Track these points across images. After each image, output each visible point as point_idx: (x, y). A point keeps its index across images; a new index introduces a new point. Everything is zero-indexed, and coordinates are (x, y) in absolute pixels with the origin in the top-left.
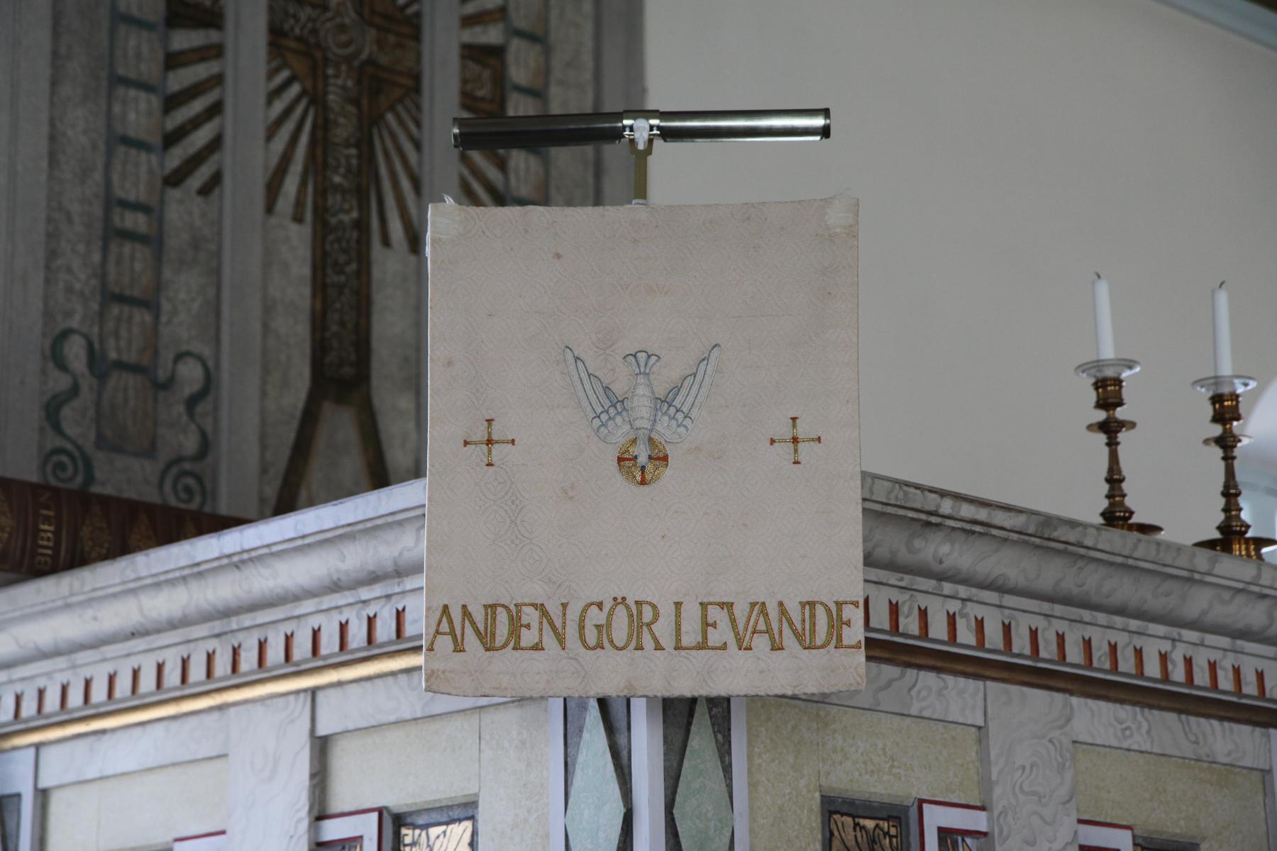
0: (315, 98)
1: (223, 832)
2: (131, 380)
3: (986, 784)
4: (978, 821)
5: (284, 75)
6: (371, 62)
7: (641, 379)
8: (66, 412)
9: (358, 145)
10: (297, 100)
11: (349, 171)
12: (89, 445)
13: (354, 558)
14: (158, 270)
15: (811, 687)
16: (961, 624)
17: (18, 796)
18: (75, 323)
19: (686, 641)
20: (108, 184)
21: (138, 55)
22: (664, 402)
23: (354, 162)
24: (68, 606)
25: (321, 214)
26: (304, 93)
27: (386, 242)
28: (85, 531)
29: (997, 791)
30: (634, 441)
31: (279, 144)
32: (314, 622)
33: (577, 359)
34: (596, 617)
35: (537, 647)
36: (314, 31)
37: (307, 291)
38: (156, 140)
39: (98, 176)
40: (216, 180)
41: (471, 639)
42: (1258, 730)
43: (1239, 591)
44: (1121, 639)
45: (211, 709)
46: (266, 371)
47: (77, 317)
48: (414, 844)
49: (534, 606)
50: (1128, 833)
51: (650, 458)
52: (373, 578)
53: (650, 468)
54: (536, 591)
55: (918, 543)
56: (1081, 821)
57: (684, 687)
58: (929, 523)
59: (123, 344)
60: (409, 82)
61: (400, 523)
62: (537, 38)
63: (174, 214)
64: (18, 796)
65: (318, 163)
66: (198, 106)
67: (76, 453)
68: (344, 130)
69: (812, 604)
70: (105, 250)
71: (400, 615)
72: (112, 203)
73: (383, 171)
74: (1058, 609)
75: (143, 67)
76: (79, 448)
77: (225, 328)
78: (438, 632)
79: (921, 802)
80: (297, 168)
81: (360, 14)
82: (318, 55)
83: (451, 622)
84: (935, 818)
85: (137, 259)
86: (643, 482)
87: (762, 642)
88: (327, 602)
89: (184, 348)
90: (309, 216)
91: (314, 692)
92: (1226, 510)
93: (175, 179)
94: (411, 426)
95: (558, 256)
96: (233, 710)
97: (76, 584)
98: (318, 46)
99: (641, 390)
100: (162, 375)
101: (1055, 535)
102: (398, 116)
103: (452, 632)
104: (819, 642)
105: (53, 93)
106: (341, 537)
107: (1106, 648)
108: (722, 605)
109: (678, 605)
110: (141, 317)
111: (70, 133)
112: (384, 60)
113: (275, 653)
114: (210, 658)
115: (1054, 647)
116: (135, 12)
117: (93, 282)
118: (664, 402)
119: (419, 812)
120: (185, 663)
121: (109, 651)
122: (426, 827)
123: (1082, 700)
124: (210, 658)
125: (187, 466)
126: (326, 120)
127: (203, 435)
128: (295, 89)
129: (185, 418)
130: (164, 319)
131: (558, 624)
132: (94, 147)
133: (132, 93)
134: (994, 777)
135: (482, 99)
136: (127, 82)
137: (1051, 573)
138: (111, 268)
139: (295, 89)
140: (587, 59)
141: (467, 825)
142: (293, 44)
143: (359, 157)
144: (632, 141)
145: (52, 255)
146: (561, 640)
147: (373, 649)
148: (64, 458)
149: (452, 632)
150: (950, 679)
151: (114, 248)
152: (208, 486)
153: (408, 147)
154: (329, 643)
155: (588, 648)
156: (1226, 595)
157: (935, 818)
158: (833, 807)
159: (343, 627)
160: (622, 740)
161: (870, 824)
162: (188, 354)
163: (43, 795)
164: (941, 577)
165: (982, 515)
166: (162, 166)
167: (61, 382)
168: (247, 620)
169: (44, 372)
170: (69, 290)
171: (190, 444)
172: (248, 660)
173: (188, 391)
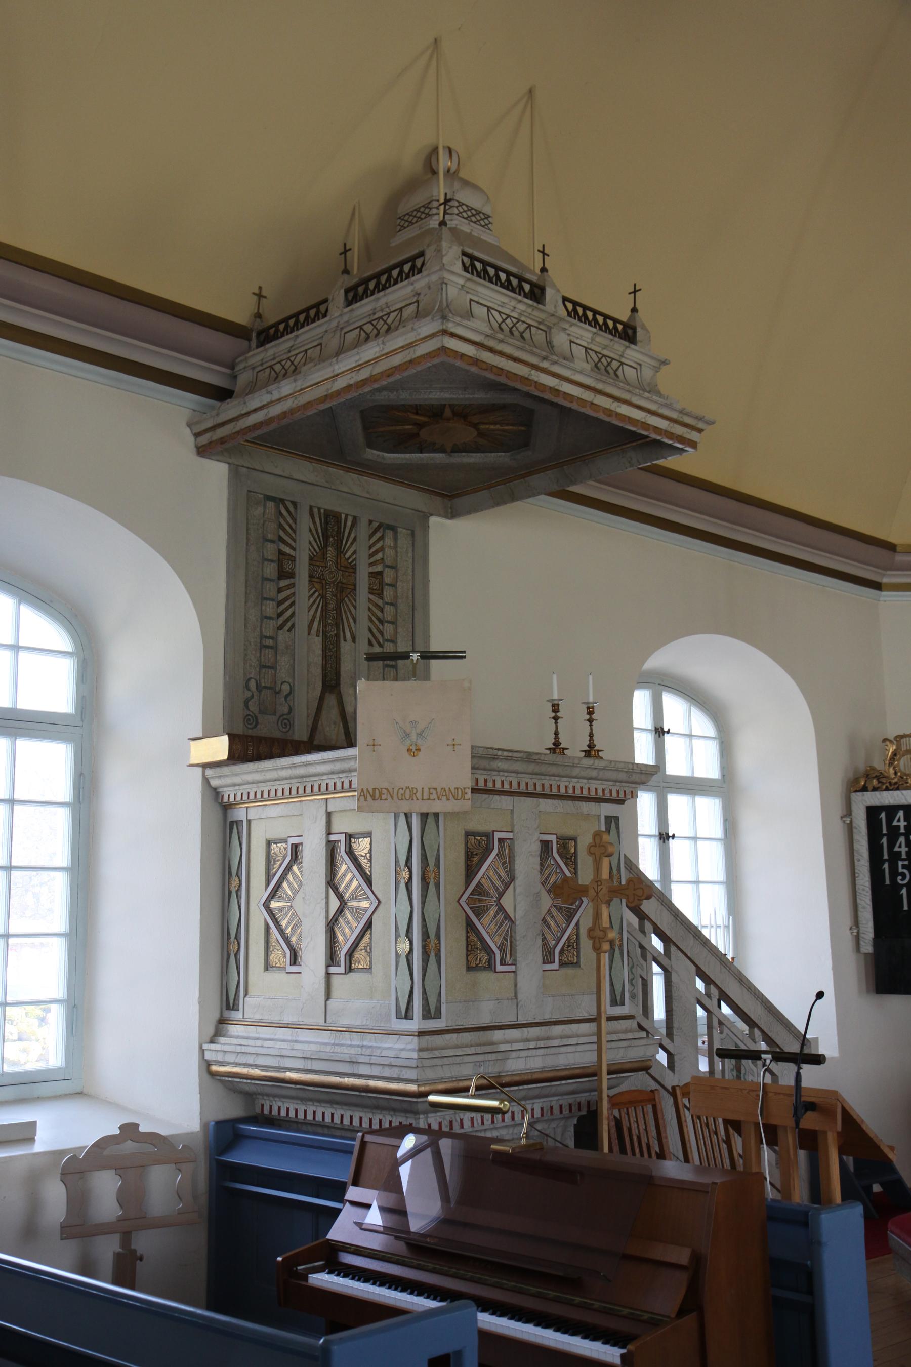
0: (323, 597)
1: (302, 836)
2: (268, 692)
3: (513, 825)
4: (510, 836)
5: (314, 590)
6: (340, 582)
7: (414, 728)
8: (250, 703)
9: (336, 610)
10: (318, 597)
11: (333, 618)
12: (257, 712)
13: (338, 766)
14: (276, 656)
15: (456, 810)
16: (505, 783)
17: (242, 821)
18: (252, 676)
19: (425, 798)
20: (261, 632)
21: (270, 590)
22: (420, 735)
23: (335, 615)
24: (257, 771)
25: (324, 633)
26: (319, 595)
27: (345, 640)
28: (261, 748)
29: (516, 827)
30: (412, 745)
31: (312, 612)
32: (327, 781)
33: (397, 723)
34: (401, 792)
35: (386, 800)
36: (323, 574)
37: (321, 658)
38: (275, 616)
39: (258, 629)
40: (293, 626)
41: (369, 798)
42: (597, 804)
43: (589, 767)
44: (553, 783)
45: (298, 801)
46: (308, 685)
47: (253, 674)
48: (355, 843)
49: (386, 789)
50: (555, 836)
51: (416, 750)
52: (343, 772)
53: (416, 752)
54: (386, 785)
55: (492, 763)
56: (540, 833)
57: (425, 810)
58: (495, 758)
59: (266, 680)
60: (352, 587)
61: (350, 759)
62: (394, 567)
63: (280, 638)
64: (242, 821)
65: (323, 618)
66: (287, 604)
67: (253, 715)
68: (332, 605)
69: (457, 788)
70: (260, 652)
71: (350, 782)
72: (263, 637)
73: (344, 617)
74: (534, 776)
75: (271, 593)
76: (254, 714)
77: (296, 673)
78: (360, 796)
79: (494, 831)
80: (317, 619)
81: (337, 567)
82: (324, 582)
83: (364, 793)
84: (497, 836)
85: (269, 653)
86: (414, 756)
87: (444, 799)
88: (330, 776)
89: (284, 680)
90: (321, 634)
91: (327, 799)
92: (590, 741)
93: (280, 628)
94: (353, 698)
95: (392, 695)
96: (304, 802)
97: (259, 766)
98: (324, 579)
99: (414, 731)
100: (277, 689)
101: (532, 758)
102: (349, 599)
103: (364, 796)
104: (459, 798)
105: (245, 605)
106: (334, 761)
107: (549, 786)
108: (434, 788)
109: (423, 788)
110: (271, 672)
111: (250, 617)
112: (344, 581)
113: (316, 789)
114: (297, 788)
115: (533, 787)
116: (269, 577)
117: (257, 662)
118: (420, 735)
119: (356, 834)
120: (290, 789)
121: (268, 784)
122: (358, 838)
123: (543, 800)
124: (297, 788)
125: (285, 717)
126: (326, 603)
127: (290, 706)
128: (317, 594)
129: (284, 702)
130: (278, 672)
131: (391, 793)
132: (257, 620)
133: (268, 602)
134: (515, 823)
135: (376, 590)
136: (266, 599)
137: (531, 767)
138: (262, 657)
139: (317, 594)
140: (410, 571)
141: (369, 838)
142: (316, 580)
143: (337, 614)
144: (413, 660)
145: (246, 655)
146: (392, 798)
147: (343, 790)
148: (250, 717)
149: (364, 796)
150: (503, 797)
151: (263, 651)
152: (292, 722)
153: (352, 608)
154: (331, 788)
155: (399, 800)
156: (584, 769)
157: (497, 836)
158: (468, 834)
159: (335, 784)
160: (409, 820)
161: (479, 838)
162: (285, 682)
163: (249, 822)
164: (499, 771)
165: (510, 754)
166: (277, 624)
167: (248, 694)
168: (308, 779)
169: (244, 692)
170: (251, 666)
171: (286, 710)
172: (308, 790)
173: (285, 693)
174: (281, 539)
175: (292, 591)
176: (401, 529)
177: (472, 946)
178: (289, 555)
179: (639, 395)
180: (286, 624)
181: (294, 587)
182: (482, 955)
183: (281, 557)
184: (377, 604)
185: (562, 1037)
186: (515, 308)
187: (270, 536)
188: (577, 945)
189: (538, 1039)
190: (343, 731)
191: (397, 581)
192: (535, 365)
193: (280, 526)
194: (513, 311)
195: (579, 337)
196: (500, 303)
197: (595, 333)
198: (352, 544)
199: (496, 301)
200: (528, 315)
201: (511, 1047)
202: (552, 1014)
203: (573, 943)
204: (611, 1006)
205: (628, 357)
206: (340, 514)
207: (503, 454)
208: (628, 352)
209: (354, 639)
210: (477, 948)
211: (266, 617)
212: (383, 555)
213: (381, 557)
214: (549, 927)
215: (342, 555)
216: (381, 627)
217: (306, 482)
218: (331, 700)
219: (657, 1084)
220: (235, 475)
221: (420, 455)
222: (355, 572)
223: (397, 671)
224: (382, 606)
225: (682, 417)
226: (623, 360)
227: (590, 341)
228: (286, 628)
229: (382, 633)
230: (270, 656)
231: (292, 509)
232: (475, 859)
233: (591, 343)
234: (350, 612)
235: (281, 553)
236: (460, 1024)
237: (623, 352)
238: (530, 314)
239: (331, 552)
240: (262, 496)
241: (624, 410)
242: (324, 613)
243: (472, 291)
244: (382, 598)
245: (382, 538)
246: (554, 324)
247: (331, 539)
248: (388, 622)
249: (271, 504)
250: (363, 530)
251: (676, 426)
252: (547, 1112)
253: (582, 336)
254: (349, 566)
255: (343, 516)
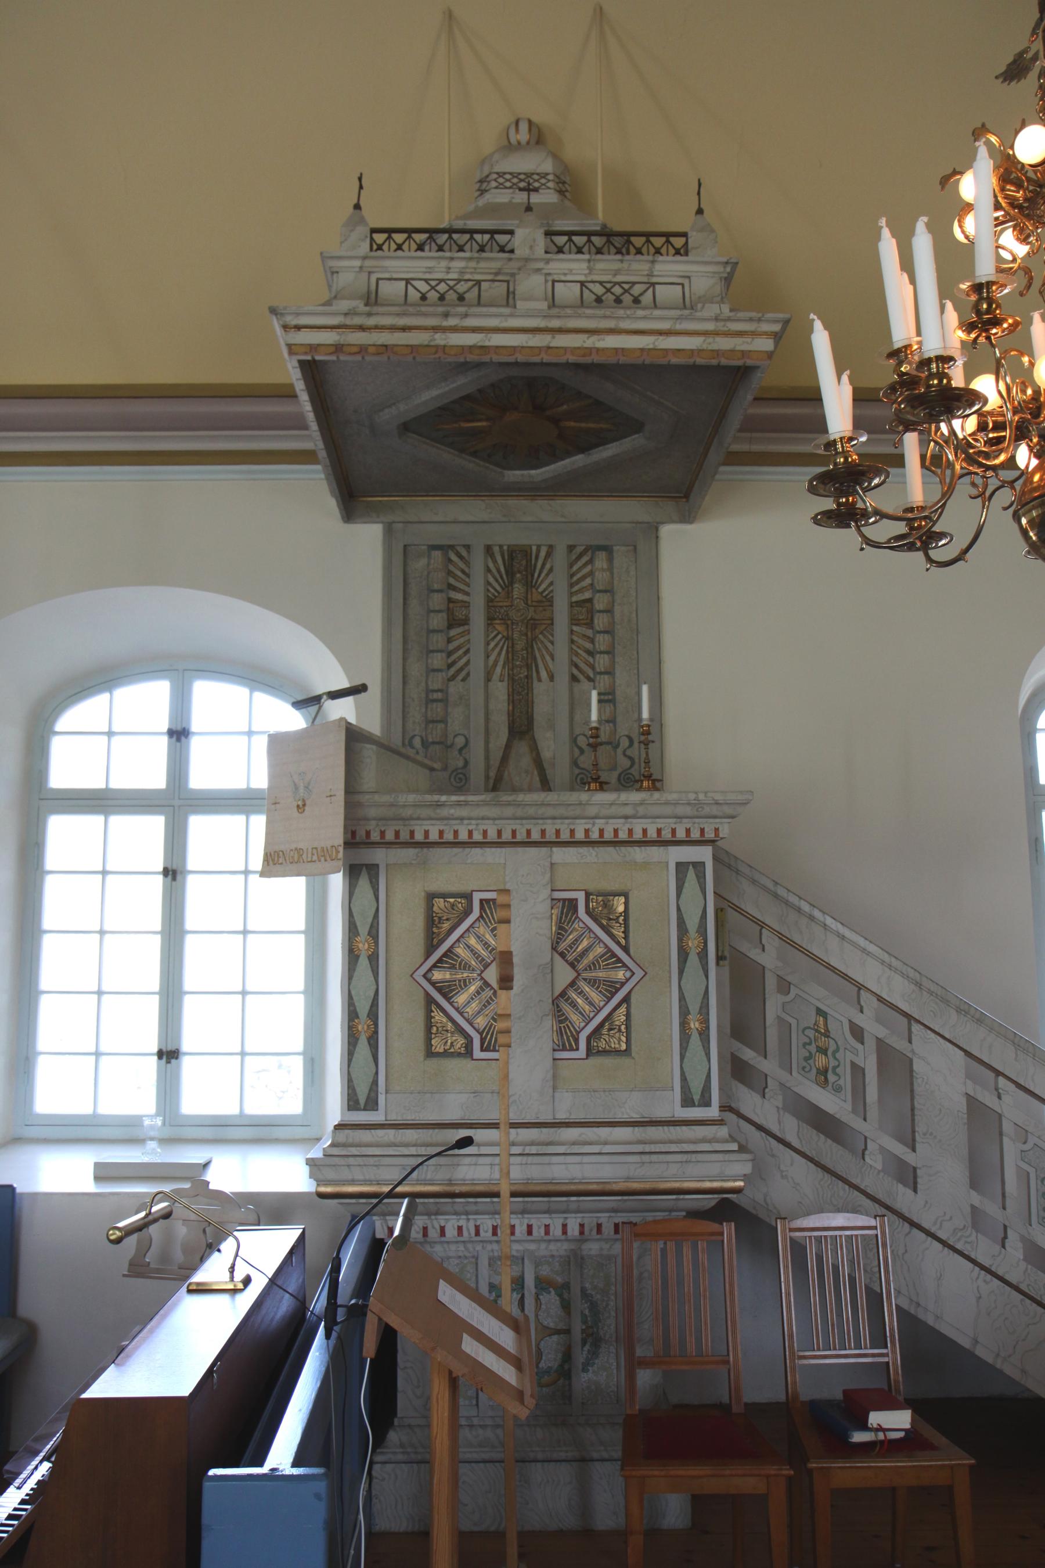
6: (532, 619)
9: (527, 649)
10: (501, 640)
18: (416, 732)
26: (503, 637)
27: (540, 680)
36: (507, 615)
62: (609, 591)
67: (455, 773)
68: (520, 645)
70: (426, 708)
72: (428, 691)
81: (527, 604)
82: (509, 622)
85: (439, 708)
87: (323, 859)
110: (441, 726)
112: (537, 617)
116: (436, 628)
125: (460, 771)
128: (500, 636)
153: (549, 645)
158: (431, 897)
161: (452, 900)
171: (461, 764)
173: (459, 747)
174: (451, 587)
175: (466, 638)
176: (618, 547)
177: (437, 1028)
178: (462, 601)
179: (628, 317)
180: (456, 671)
181: (469, 633)
182: (454, 1038)
183: (451, 605)
184: (584, 636)
185: (574, 1143)
186: (449, 268)
187: (436, 587)
188: (627, 1028)
189: (532, 1144)
190: (538, 779)
191: (613, 606)
192: (437, 326)
193: (450, 573)
194: (448, 273)
195: (566, 272)
196: (424, 270)
197: (589, 261)
198: (547, 575)
199: (419, 270)
200: (473, 270)
201: (479, 1150)
202: (570, 1114)
203: (620, 1026)
204: (682, 1107)
205: (660, 273)
206: (530, 546)
207: (637, 436)
208: (659, 268)
209: (552, 678)
210: (447, 1031)
211: (434, 670)
212: (593, 580)
213: (590, 582)
214: (575, 1005)
215: (534, 590)
216: (591, 660)
217: (478, 522)
218: (522, 748)
219: (877, 1206)
220: (389, 531)
221: (563, 462)
222: (552, 606)
223: (615, 706)
224: (591, 636)
225: (724, 326)
226: (654, 280)
227: (587, 272)
228: (460, 677)
229: (592, 667)
230: (439, 710)
231: (464, 553)
232: (445, 925)
233: (590, 274)
234: (546, 648)
235: (450, 600)
236: (409, 1118)
237: (651, 270)
238: (475, 269)
239: (518, 589)
240: (425, 547)
241: (611, 342)
242: (510, 655)
243: (377, 269)
244: (592, 628)
245: (591, 561)
246: (519, 269)
247: (518, 575)
248: (601, 653)
249: (437, 554)
250: (560, 558)
251: (718, 339)
252: (591, 1230)
253: (571, 270)
254: (544, 599)
255: (534, 548)
